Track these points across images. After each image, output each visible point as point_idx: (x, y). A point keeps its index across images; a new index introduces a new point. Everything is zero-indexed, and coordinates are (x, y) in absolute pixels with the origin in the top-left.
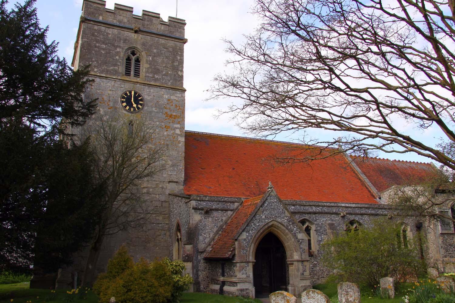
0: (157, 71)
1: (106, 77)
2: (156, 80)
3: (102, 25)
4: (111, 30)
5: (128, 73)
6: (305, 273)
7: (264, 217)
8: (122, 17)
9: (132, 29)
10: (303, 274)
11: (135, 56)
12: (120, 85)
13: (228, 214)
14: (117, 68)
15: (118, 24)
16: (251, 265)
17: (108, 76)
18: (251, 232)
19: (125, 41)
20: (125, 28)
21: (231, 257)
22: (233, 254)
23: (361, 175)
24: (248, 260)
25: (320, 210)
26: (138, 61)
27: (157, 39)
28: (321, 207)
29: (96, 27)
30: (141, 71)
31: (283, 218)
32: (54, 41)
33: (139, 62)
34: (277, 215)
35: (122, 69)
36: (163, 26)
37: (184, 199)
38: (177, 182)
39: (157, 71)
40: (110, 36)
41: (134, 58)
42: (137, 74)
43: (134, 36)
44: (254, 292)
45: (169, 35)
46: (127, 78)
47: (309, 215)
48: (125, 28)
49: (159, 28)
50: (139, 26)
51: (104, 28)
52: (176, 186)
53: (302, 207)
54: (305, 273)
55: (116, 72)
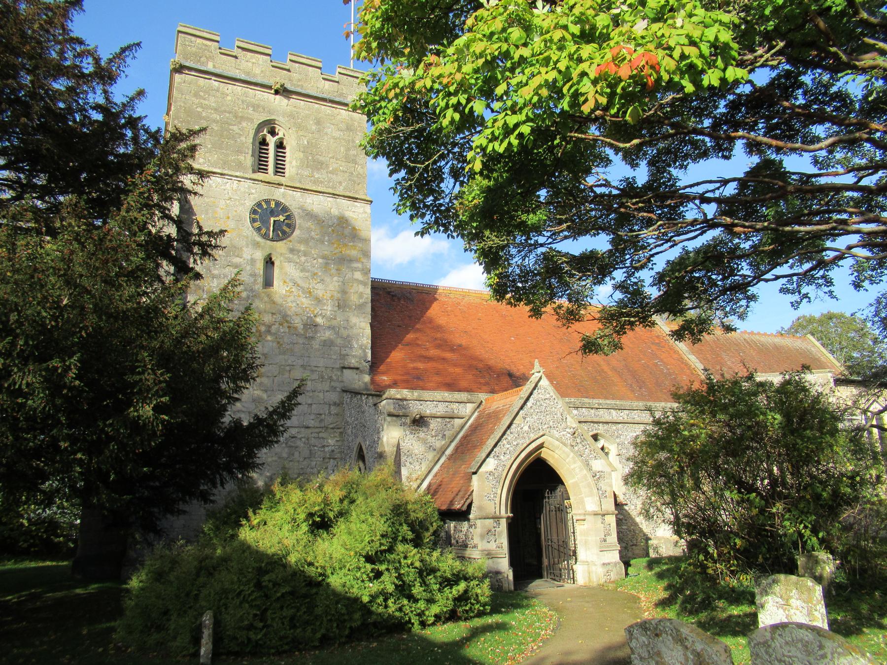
0: (319, 165)
1: (221, 174)
2: (316, 182)
3: (214, 78)
4: (230, 87)
5: (260, 165)
6: (608, 538)
7: (526, 428)
8: (250, 64)
9: (270, 88)
10: (605, 540)
11: (277, 137)
12: (249, 188)
13: (455, 426)
14: (243, 158)
15: (419, 481)
16: (504, 523)
17: (226, 172)
18: (502, 457)
19: (256, 107)
20: (256, 84)
21: (465, 508)
22: (469, 501)
23: (690, 357)
24: (498, 513)
25: (625, 417)
26: (280, 145)
27: (317, 106)
28: (627, 412)
29: (201, 82)
30: (287, 167)
31: (564, 429)
32: (226, 231)
33: (284, 148)
34: (551, 424)
35: (248, 160)
36: (327, 82)
37: (370, 397)
38: (357, 369)
39: (319, 165)
40: (229, 98)
41: (272, 141)
42: (279, 169)
43: (269, 97)
44: (511, 577)
45: (337, 99)
46: (260, 176)
47: (606, 426)
48: (256, 84)
49: (321, 86)
50: (283, 82)
51: (216, 84)
52: (357, 377)
53: (593, 411)
54: (608, 538)
55: (240, 166)
